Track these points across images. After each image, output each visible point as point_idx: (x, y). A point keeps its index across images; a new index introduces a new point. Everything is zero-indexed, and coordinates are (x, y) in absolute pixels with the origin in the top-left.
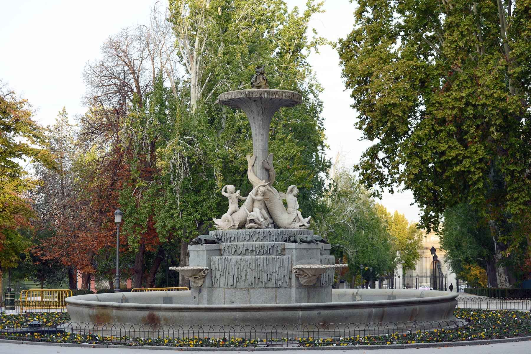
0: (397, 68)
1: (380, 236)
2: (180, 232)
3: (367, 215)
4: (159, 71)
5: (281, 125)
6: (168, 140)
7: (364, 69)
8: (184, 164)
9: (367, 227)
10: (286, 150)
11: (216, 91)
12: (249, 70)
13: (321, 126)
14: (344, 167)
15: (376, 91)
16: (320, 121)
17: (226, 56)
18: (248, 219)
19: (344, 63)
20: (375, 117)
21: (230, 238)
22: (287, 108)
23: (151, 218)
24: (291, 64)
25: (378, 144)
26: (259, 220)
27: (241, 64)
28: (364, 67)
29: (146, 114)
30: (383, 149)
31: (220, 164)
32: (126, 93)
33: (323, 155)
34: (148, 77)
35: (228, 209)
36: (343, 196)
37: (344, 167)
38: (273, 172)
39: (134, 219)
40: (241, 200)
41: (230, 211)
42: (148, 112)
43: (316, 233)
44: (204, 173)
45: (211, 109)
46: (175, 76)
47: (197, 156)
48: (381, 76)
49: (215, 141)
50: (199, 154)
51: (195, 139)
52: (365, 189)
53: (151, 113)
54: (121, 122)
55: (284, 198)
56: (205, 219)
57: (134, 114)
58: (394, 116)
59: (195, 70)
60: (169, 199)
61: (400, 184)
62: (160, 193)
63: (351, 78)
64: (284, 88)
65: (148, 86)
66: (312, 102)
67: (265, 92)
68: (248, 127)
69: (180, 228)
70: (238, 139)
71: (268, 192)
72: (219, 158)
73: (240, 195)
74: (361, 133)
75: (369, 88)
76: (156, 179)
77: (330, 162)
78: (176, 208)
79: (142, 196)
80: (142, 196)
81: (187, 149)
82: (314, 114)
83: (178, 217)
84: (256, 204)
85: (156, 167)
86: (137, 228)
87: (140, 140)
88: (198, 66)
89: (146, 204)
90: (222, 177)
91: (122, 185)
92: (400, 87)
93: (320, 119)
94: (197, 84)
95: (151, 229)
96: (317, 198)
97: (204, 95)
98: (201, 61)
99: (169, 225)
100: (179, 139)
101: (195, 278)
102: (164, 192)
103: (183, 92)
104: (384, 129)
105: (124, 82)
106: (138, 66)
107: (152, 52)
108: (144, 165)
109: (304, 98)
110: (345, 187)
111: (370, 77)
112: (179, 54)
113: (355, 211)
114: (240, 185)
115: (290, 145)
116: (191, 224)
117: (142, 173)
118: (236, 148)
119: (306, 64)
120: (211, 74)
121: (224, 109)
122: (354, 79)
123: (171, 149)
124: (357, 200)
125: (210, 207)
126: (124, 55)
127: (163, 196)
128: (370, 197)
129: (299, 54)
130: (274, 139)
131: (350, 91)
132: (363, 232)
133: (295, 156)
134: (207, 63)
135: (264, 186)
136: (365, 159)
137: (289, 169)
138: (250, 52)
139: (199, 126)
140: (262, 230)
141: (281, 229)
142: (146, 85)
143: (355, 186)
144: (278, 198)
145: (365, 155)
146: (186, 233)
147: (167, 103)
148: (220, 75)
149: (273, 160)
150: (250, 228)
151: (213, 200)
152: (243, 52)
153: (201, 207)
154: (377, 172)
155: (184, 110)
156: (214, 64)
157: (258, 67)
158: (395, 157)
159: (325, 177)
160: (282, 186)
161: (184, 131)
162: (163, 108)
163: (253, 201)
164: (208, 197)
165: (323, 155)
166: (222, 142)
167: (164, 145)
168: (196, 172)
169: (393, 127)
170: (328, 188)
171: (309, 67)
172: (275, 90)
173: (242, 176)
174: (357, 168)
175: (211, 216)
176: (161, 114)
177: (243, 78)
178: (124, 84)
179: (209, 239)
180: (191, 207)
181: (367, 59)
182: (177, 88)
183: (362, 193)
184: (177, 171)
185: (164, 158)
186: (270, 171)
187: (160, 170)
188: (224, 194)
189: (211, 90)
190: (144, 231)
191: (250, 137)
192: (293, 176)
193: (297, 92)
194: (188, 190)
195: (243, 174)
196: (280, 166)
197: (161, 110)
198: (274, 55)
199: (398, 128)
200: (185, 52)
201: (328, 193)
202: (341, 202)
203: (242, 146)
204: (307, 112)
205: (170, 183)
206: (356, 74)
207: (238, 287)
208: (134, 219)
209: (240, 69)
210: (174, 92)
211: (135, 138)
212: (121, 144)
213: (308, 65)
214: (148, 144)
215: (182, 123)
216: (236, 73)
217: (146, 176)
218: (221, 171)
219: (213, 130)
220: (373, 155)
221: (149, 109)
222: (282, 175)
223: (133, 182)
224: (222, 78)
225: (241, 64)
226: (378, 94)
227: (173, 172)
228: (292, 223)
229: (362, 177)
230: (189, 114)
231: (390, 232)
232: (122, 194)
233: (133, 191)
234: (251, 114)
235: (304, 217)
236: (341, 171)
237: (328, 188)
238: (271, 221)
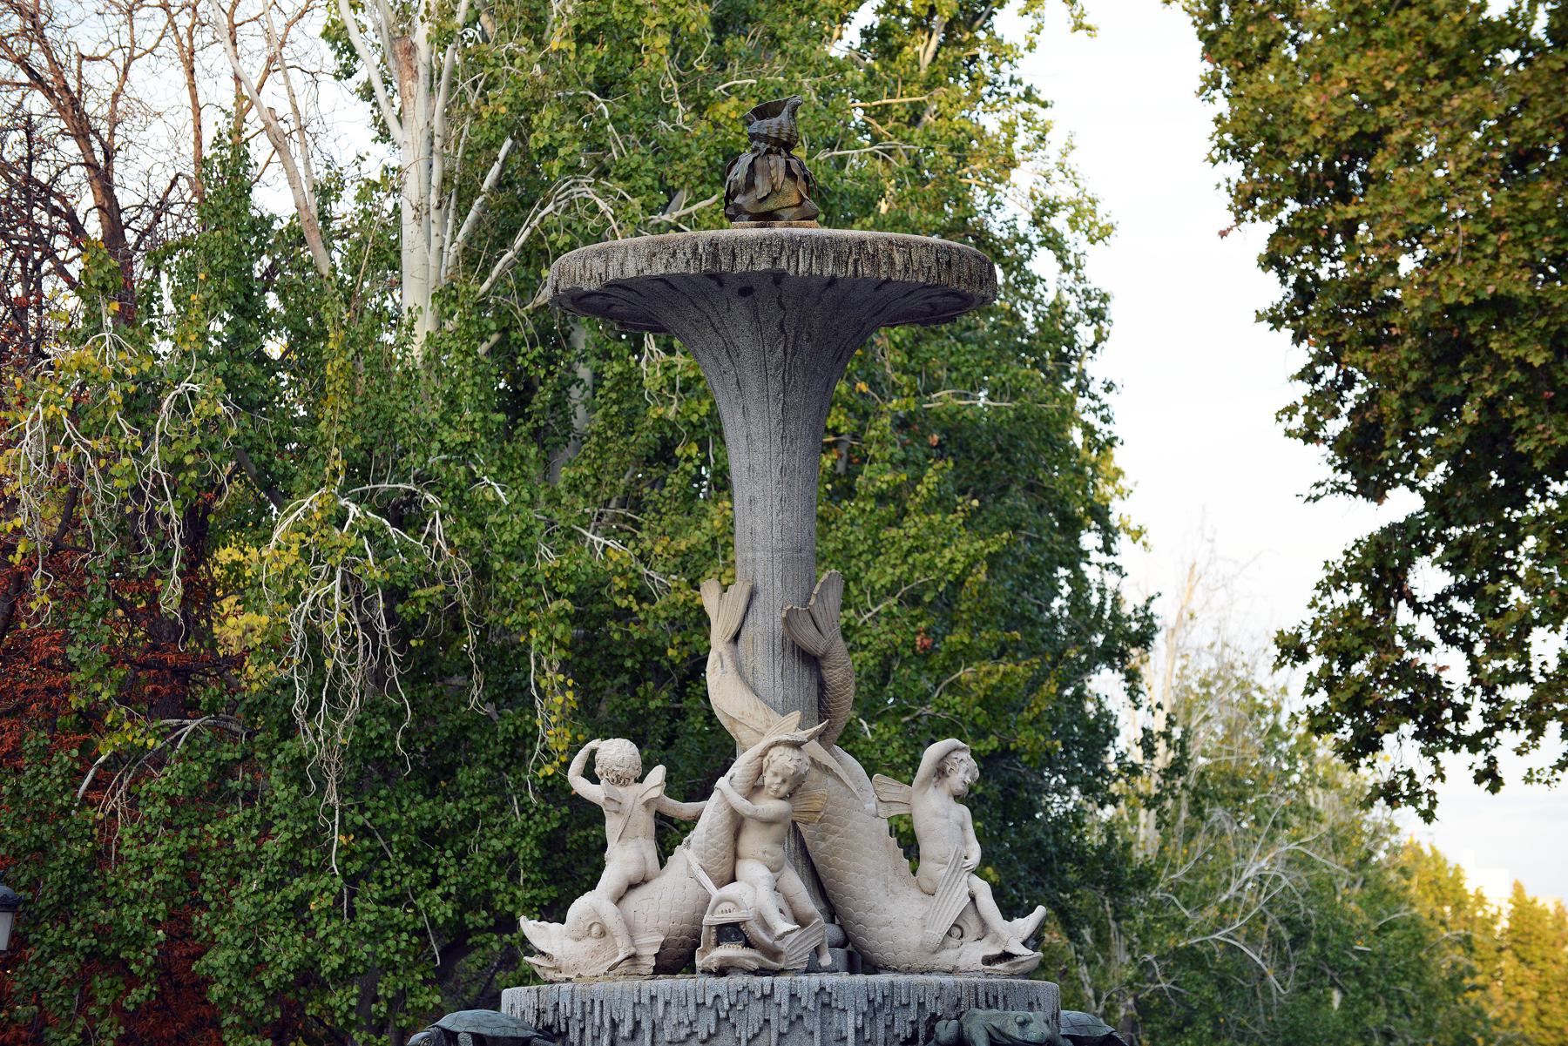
0: (1524, 104)
1: (1429, 1024)
2: (342, 999)
3: (1353, 906)
4: (225, 125)
5: (886, 420)
6: (282, 499)
7: (1337, 111)
8: (366, 626)
9: (1358, 972)
10: (909, 552)
11: (536, 238)
12: (716, 125)
13: (1097, 424)
14: (1226, 645)
15: (1400, 233)
16: (1093, 397)
17: (589, 50)
18: (708, 919)
19: (1225, 80)
20: (1395, 372)
21: (615, 1025)
22: (916, 329)
23: (179, 925)
24: (938, 92)
25: (1411, 520)
26: (767, 927)
27: (670, 91)
28: (1334, 101)
29: (157, 356)
30: (1440, 548)
31: (559, 630)
32: (41, 240)
33: (1111, 580)
34: (163, 157)
35: (601, 867)
36: (1219, 798)
37: (1226, 645)
38: (842, 671)
39: (82, 933)
40: (670, 820)
41: (611, 878)
42: (165, 347)
43: (1072, 999)
44: (477, 677)
45: (514, 335)
46: (317, 156)
47: (435, 582)
48: (1428, 150)
49: (532, 504)
50: (447, 577)
51: (429, 496)
52: (1338, 760)
53: (185, 354)
54: (14, 401)
55: (903, 810)
56: (481, 922)
57: (88, 355)
58: (1501, 365)
59: (422, 122)
60: (283, 817)
61: (1534, 737)
62: (234, 784)
63: (1263, 162)
64: (900, 222)
65: (163, 206)
66: (1050, 298)
67: (796, 244)
68: (709, 432)
69: (342, 976)
70: (655, 497)
71: (815, 774)
72: (558, 596)
73: (668, 792)
74: (1317, 462)
75: (1359, 218)
76: (212, 709)
77: (1150, 617)
78: (323, 867)
79: (133, 805)
80: (133, 805)
81: (385, 546)
82: (1065, 358)
83: (330, 914)
84: (753, 841)
85: (214, 644)
86: (100, 982)
87: (125, 501)
88: (440, 101)
89: (153, 847)
90: (570, 695)
91: (19, 742)
92: (1535, 206)
93: (1095, 388)
94: (434, 200)
95: (178, 985)
96: (1078, 806)
97: (473, 259)
98: (453, 73)
99: (284, 959)
100: (343, 492)
102: (254, 782)
103: (359, 244)
104: (1446, 440)
105: (29, 178)
106: (108, 95)
107: (184, 21)
108: (148, 634)
109: (1007, 274)
110: (1230, 753)
111: (1368, 158)
112: (336, 35)
113: (1285, 882)
114: (670, 740)
115: (931, 526)
116: (404, 953)
117: (136, 679)
118: (648, 544)
119: (1021, 90)
120: (513, 148)
121: (583, 336)
122: (1280, 166)
123: (295, 548)
124: (1295, 820)
125: (506, 860)
126: (24, 31)
127: (249, 799)
128: (1368, 803)
129: (981, 35)
130: (849, 492)
131: (1259, 234)
132: (1336, 997)
133: (959, 583)
134: (487, 87)
135: (797, 745)
136: (1340, 598)
137: (928, 652)
138: (720, 26)
139: (449, 423)
140: (782, 981)
141: (884, 978)
142: (154, 202)
143: (1283, 746)
144: (871, 806)
145: (1336, 581)
146: (376, 999)
147: (272, 301)
148: (561, 152)
149: (844, 607)
150: (722, 972)
151: (521, 818)
152: (683, 29)
153: (460, 856)
154: (1407, 674)
155: (369, 341)
156: (527, 93)
157: (763, 112)
158: (1508, 591)
159: (1124, 697)
160: (888, 743)
161: (370, 452)
162: (252, 327)
163: (738, 824)
164: (494, 806)
165: (1111, 580)
166: (574, 509)
167: (257, 525)
168: (433, 668)
169: (1496, 429)
170: (1136, 756)
171: (1035, 107)
172: (854, 233)
173: (680, 693)
174: (1292, 650)
175: (509, 908)
176: (241, 359)
177: (681, 167)
178: (27, 191)
179: (498, 1032)
180: (407, 860)
181: (1353, 58)
182: (325, 219)
183: (1324, 785)
184: (329, 664)
185: (260, 598)
186: (825, 664)
187: (238, 661)
188: (581, 786)
189: (513, 233)
190: (137, 995)
191: (722, 483)
192: (953, 688)
193: (970, 246)
194: (387, 768)
195: (686, 678)
196: (882, 635)
197: (239, 336)
198: (845, 42)
199: (1522, 431)
200: (370, 26)
201: (1138, 781)
202: (1211, 830)
203: (677, 530)
204: (1021, 348)
205: (289, 729)
206: (1291, 141)
208: (82, 933)
209: (668, 120)
210: (313, 238)
211: (95, 487)
212: (19, 522)
213: (1028, 96)
214: (167, 519)
215: (358, 410)
216: (645, 141)
217: (155, 692)
218: (565, 667)
219: (521, 446)
220: (1383, 579)
221: (172, 331)
222: (890, 686)
223: (85, 728)
224: (572, 169)
225: (670, 91)
226: (1413, 249)
227: (308, 671)
228: (943, 945)
229: (1322, 696)
230: (392, 359)
231: (1491, 1001)
232: (17, 791)
233: (82, 775)
234: (726, 363)
235: (1011, 910)
236: (1208, 663)
237: (1136, 756)
238: (833, 932)
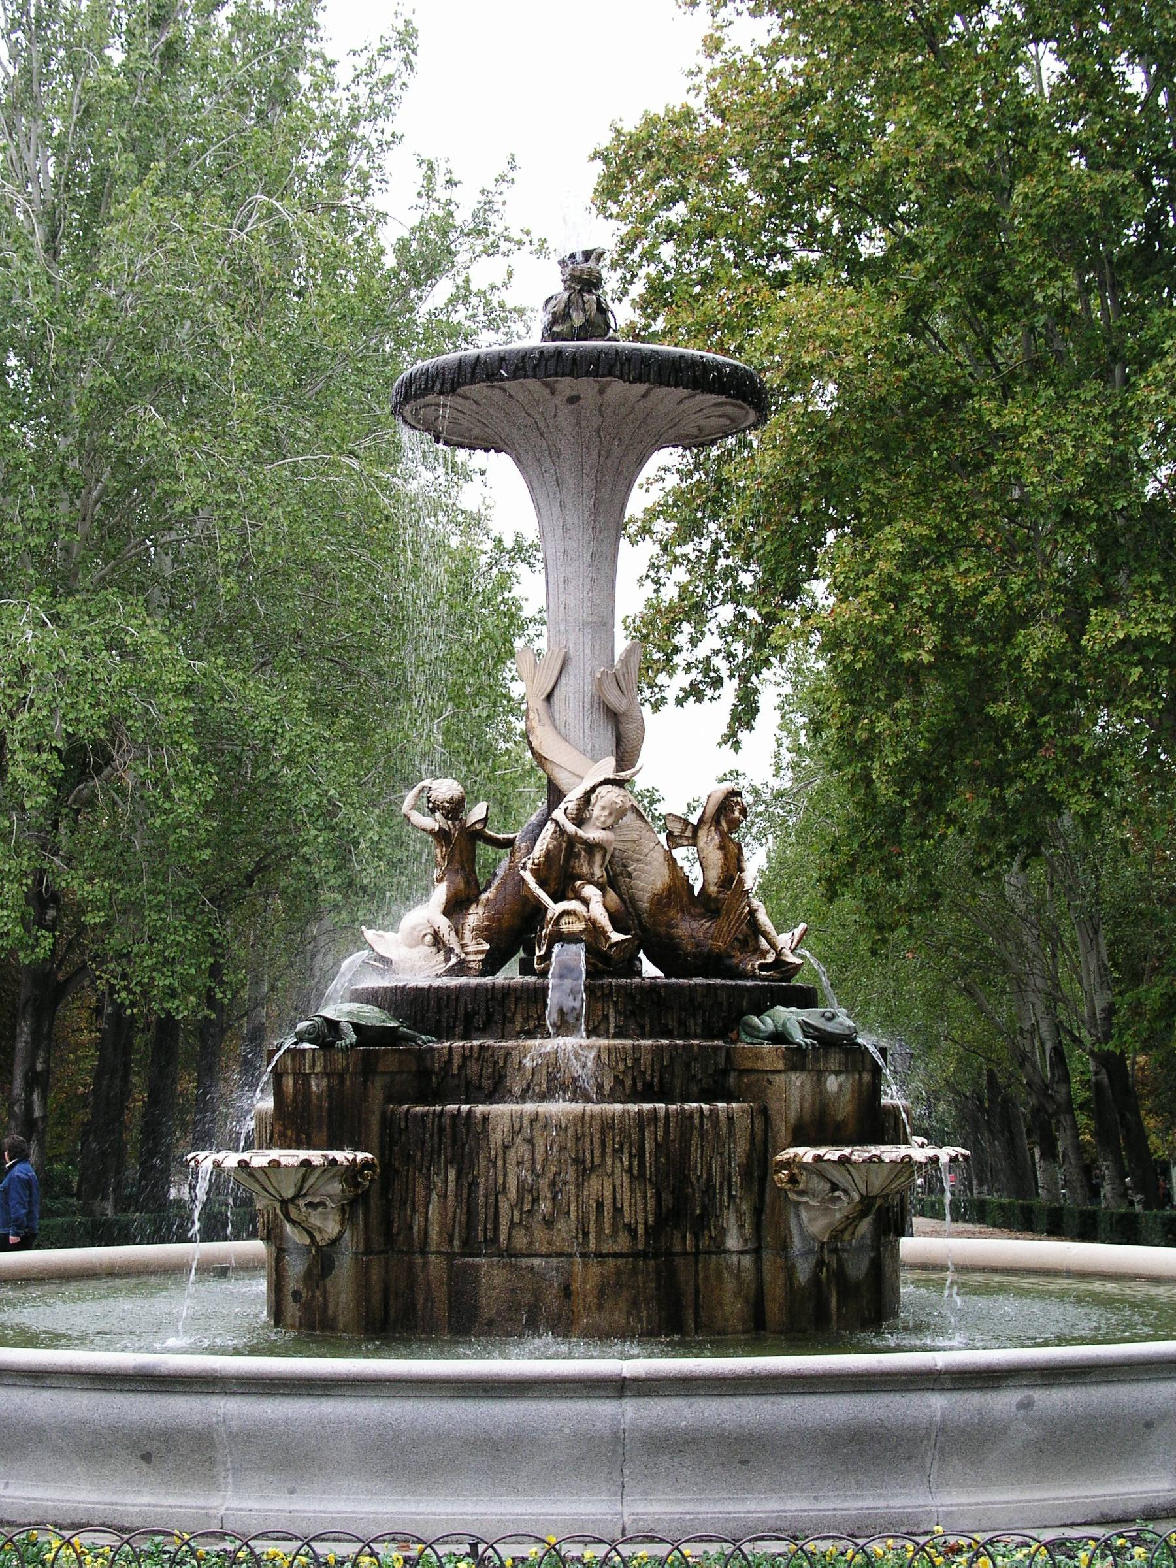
101: (310, 1205)
186: (623, 720)
234: (547, 464)
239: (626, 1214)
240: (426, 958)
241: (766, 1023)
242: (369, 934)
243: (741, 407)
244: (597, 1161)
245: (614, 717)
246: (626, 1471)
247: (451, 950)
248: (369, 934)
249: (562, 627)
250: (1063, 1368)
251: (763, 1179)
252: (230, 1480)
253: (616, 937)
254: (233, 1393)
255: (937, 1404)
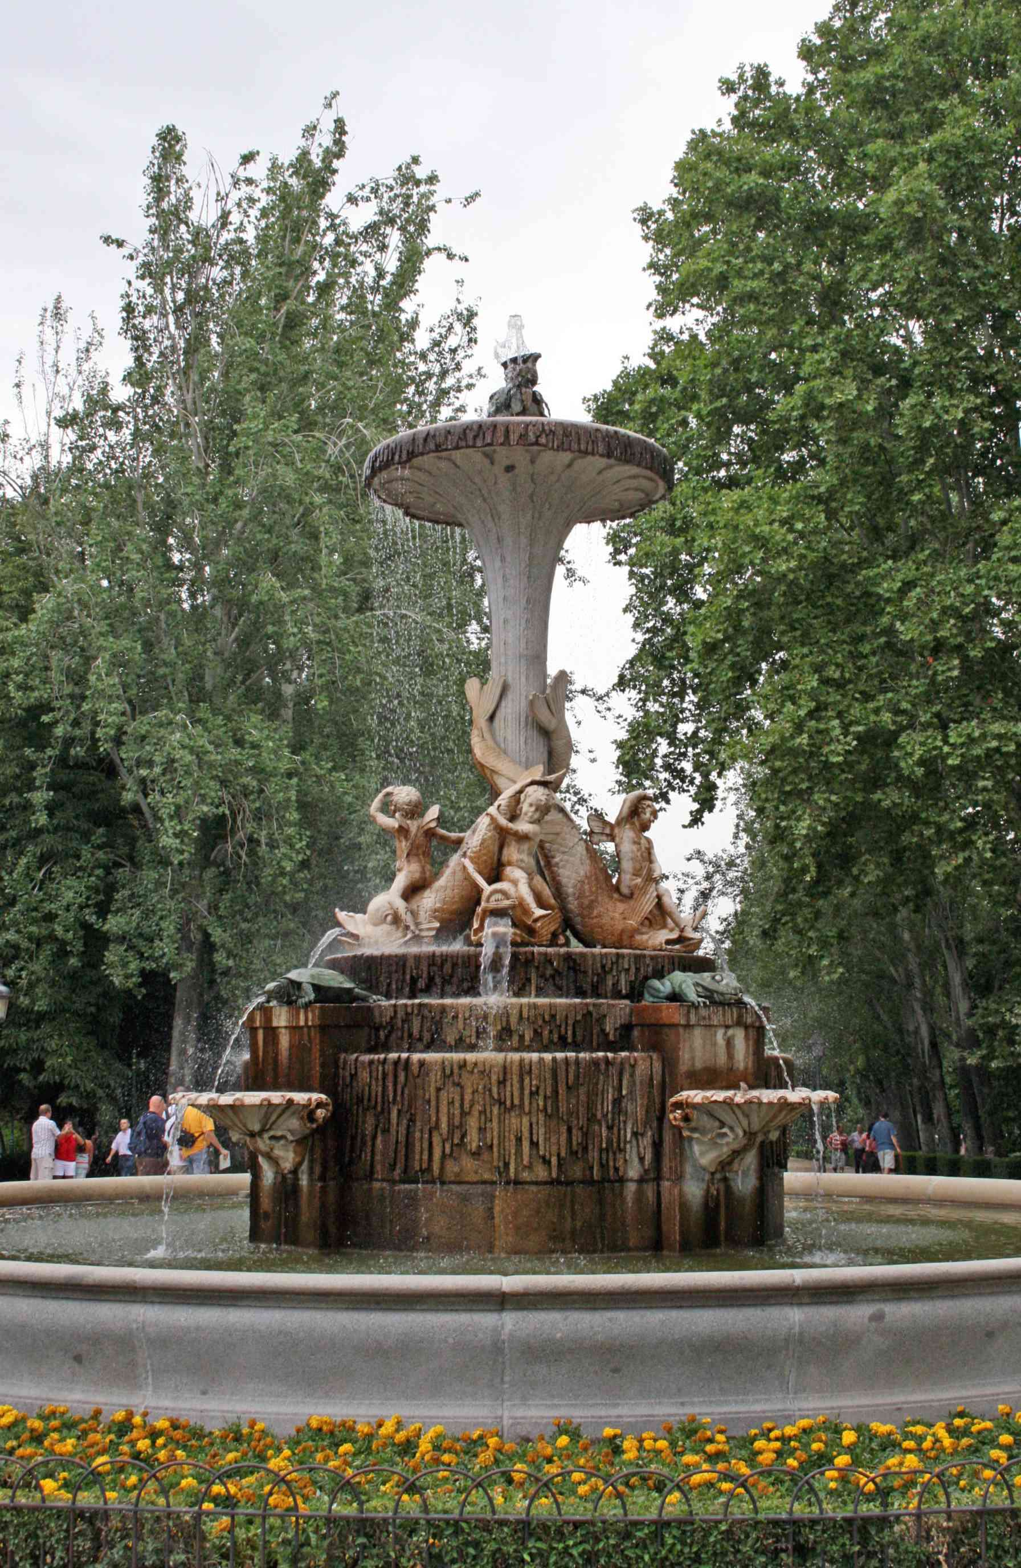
101: (272, 1138)
186: (554, 737)
207: (449, 1176)
208: (824, 1531)
234: (490, 525)
239: (541, 1148)
240: (389, 934)
241: (664, 986)
242: (341, 915)
243: (651, 479)
244: (516, 1102)
245: (545, 733)
246: (507, 1379)
247: (407, 927)
248: (341, 915)
249: (503, 660)
250: (912, 1284)
251: (661, 1118)
252: (150, 1380)
253: (539, 912)
254: (152, 1302)
255: (795, 1316)
